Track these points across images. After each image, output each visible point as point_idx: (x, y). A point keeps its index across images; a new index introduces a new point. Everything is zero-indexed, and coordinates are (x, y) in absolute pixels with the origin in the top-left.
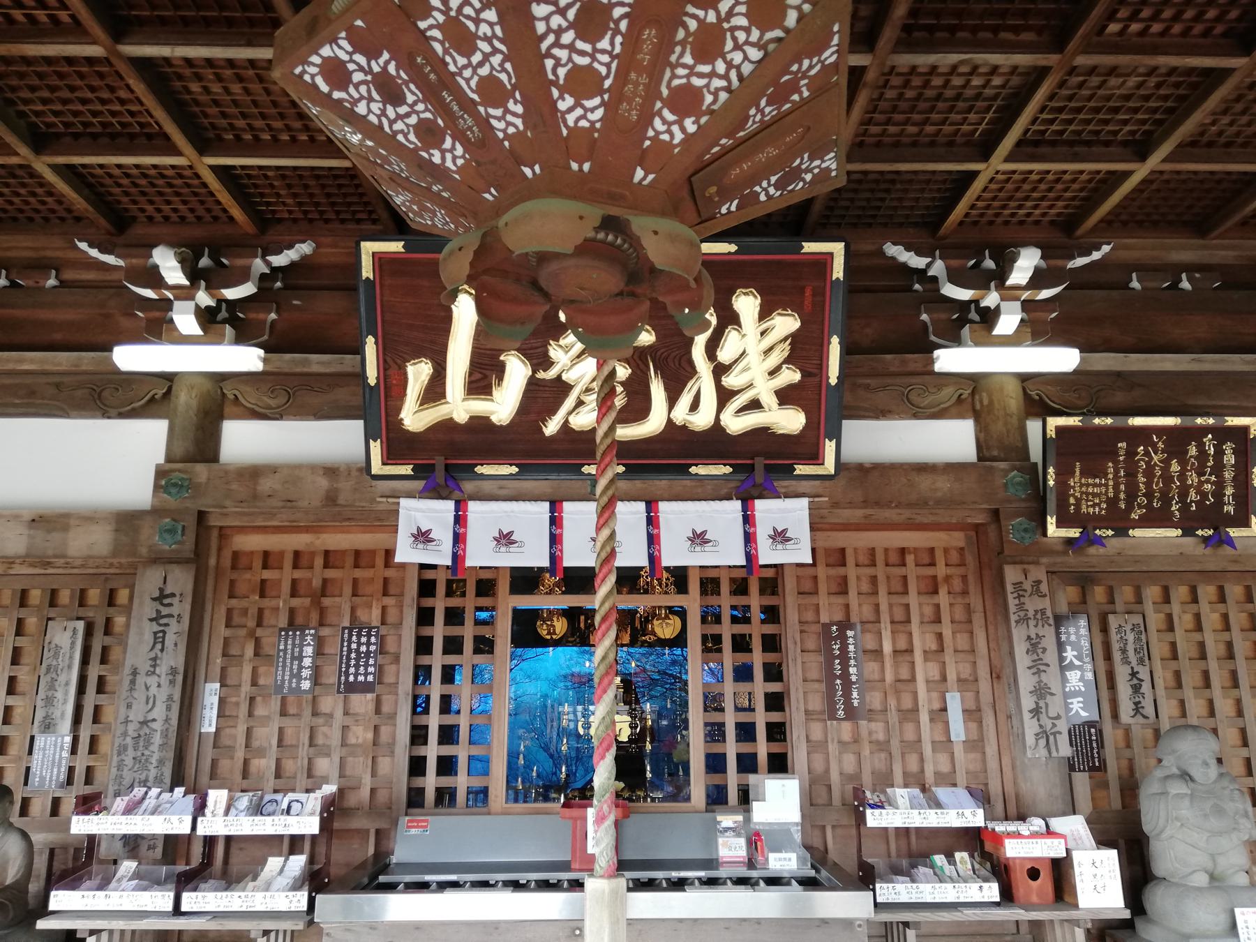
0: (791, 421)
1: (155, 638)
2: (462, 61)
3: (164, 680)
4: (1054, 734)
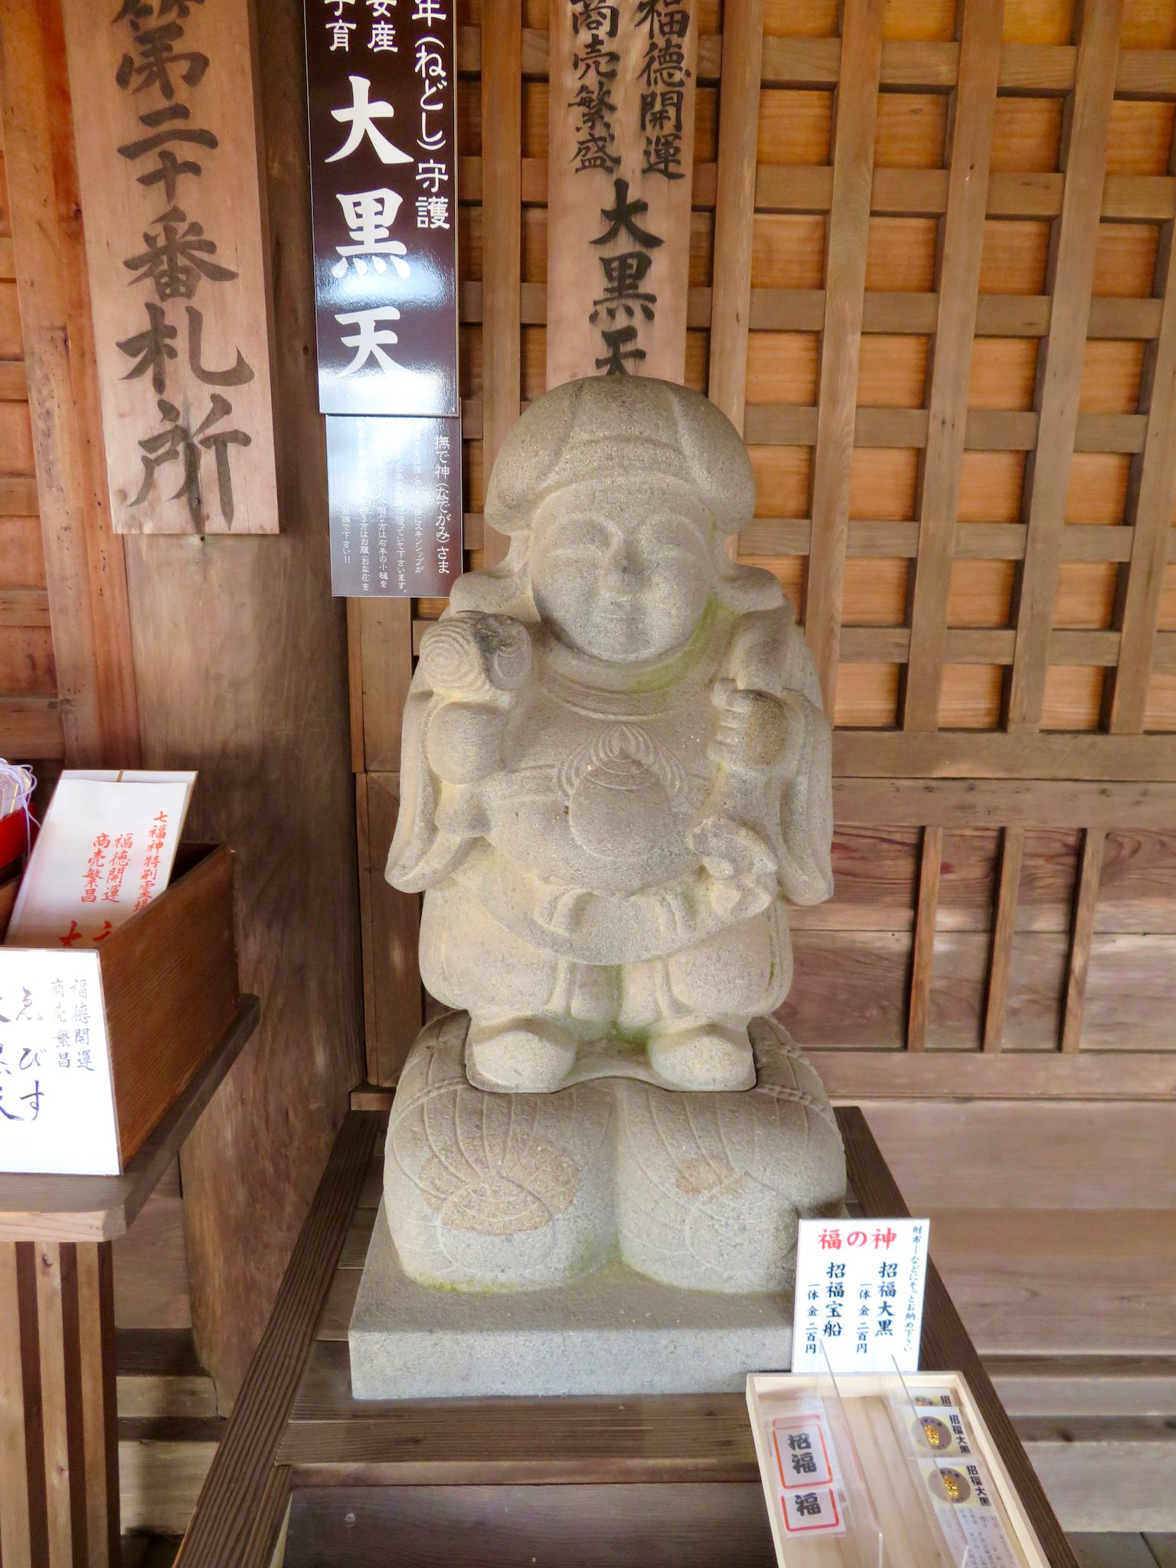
4: (219, 443)
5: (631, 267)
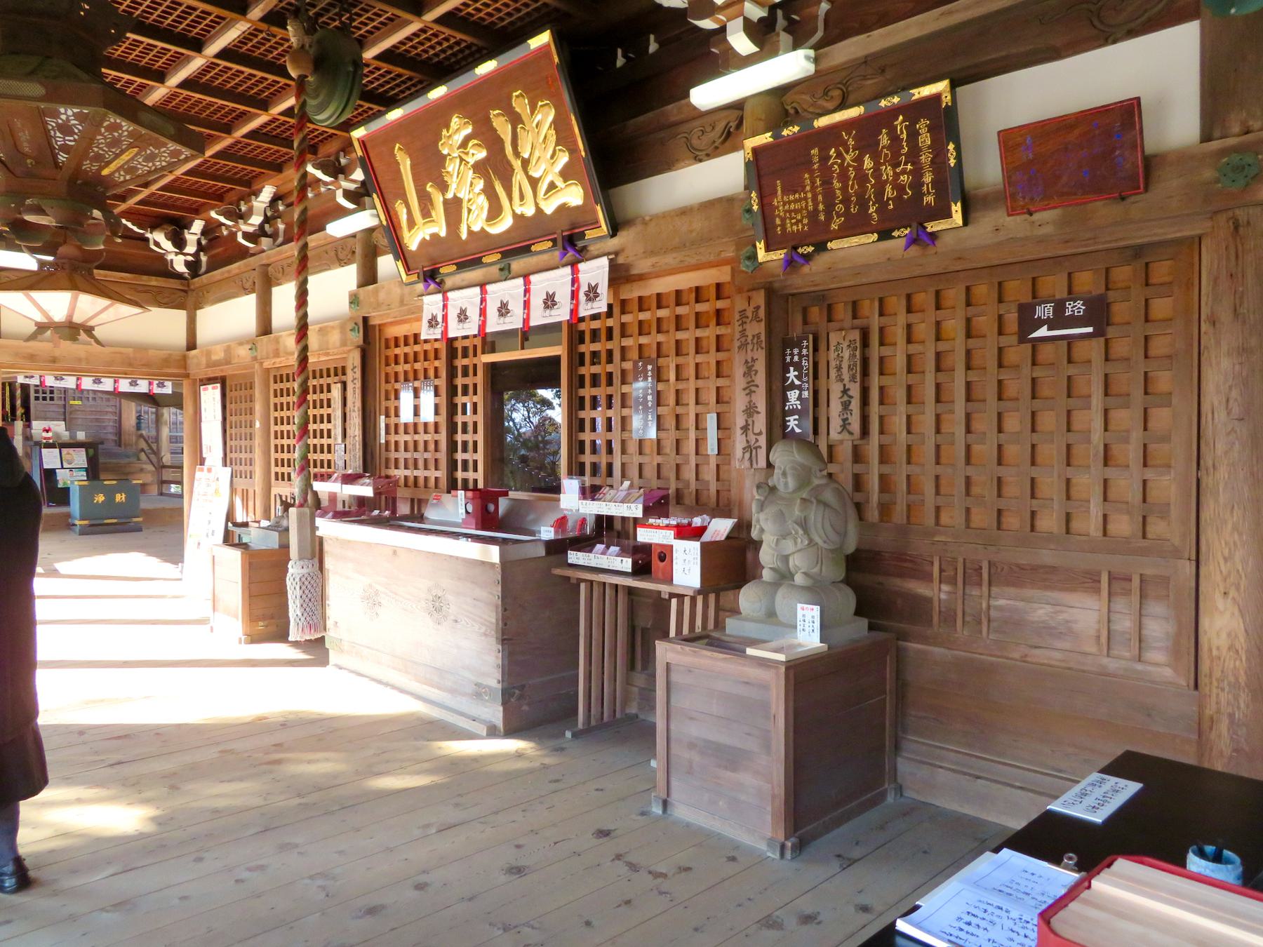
5: (161, 385)
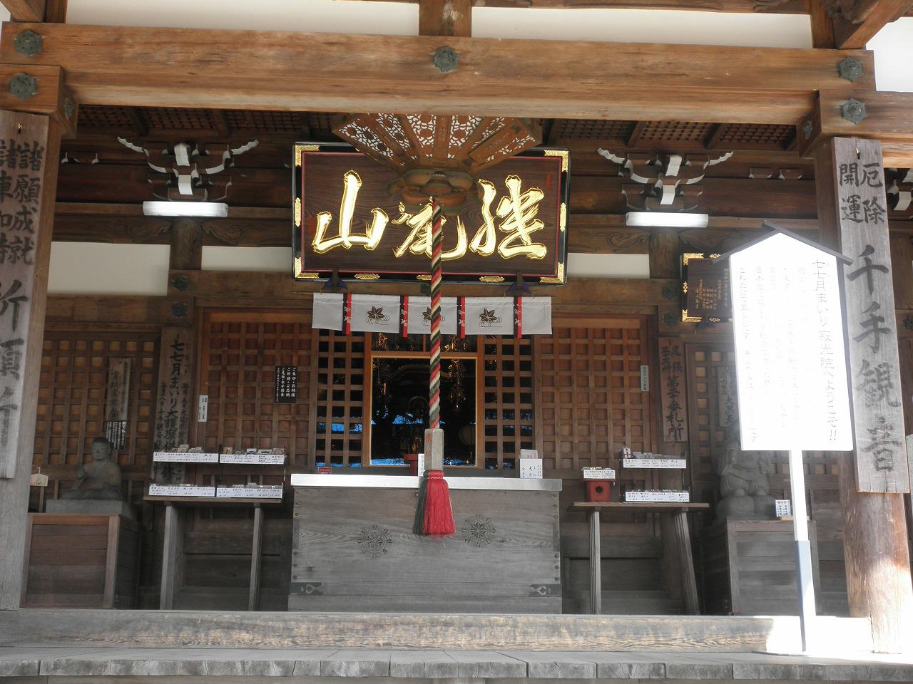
0: (539, 251)
1: (174, 367)
2: (389, 129)
3: (181, 392)
4: (679, 429)
